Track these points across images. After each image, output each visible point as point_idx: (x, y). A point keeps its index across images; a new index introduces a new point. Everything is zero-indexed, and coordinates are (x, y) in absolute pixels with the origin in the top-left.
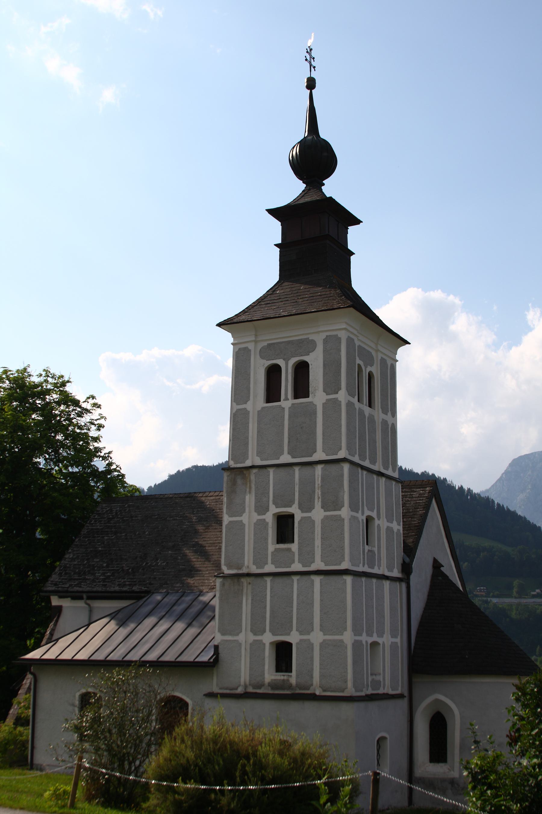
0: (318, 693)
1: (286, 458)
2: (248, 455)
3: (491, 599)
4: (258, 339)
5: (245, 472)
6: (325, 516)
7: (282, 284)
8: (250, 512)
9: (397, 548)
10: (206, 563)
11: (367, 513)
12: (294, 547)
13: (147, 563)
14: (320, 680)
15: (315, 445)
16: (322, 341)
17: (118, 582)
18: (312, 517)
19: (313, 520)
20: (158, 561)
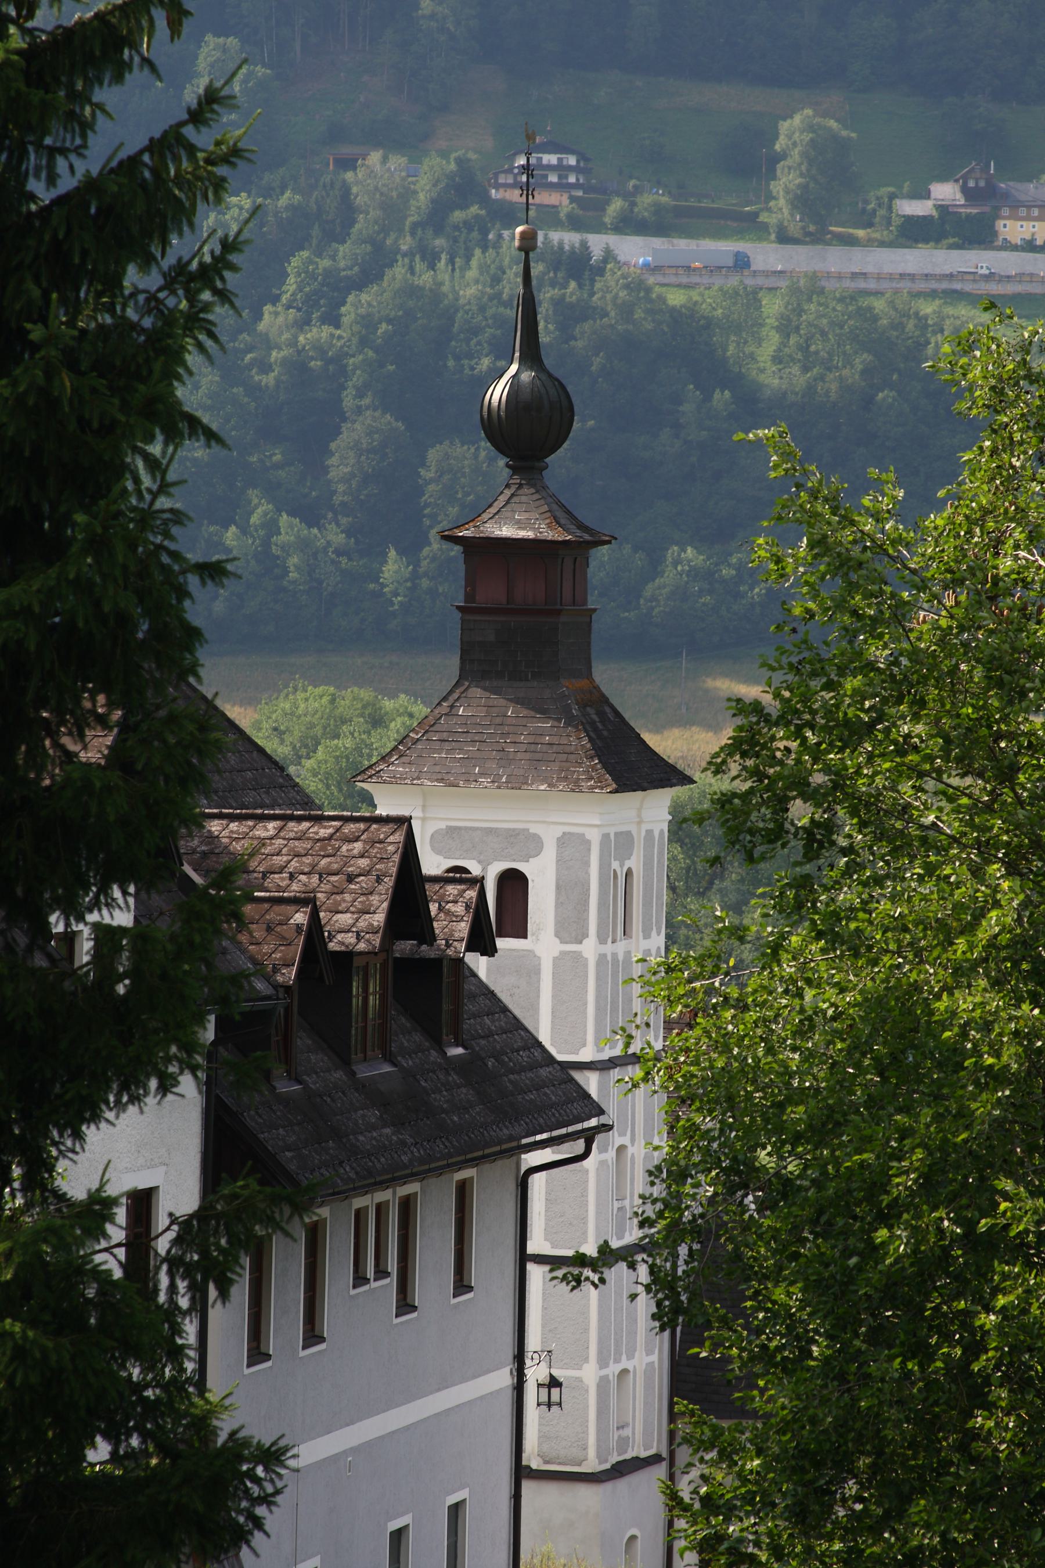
3: (612, 240)
14: (540, 1444)
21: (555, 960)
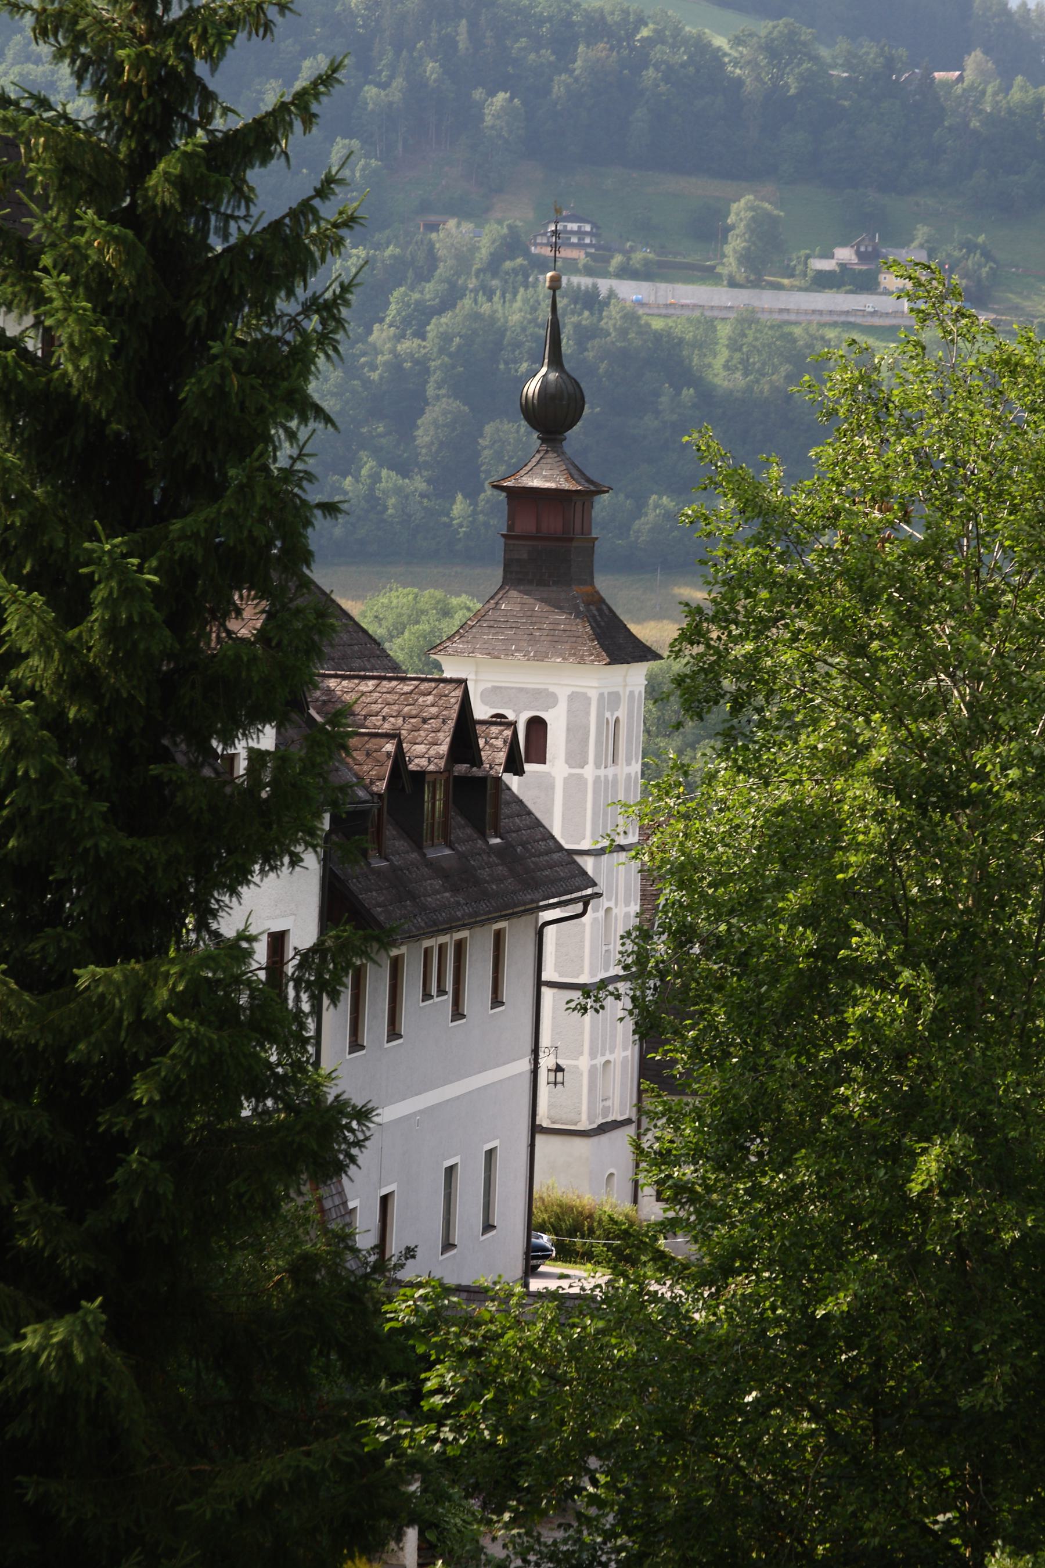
0: (545, 1125)
3: (614, 283)
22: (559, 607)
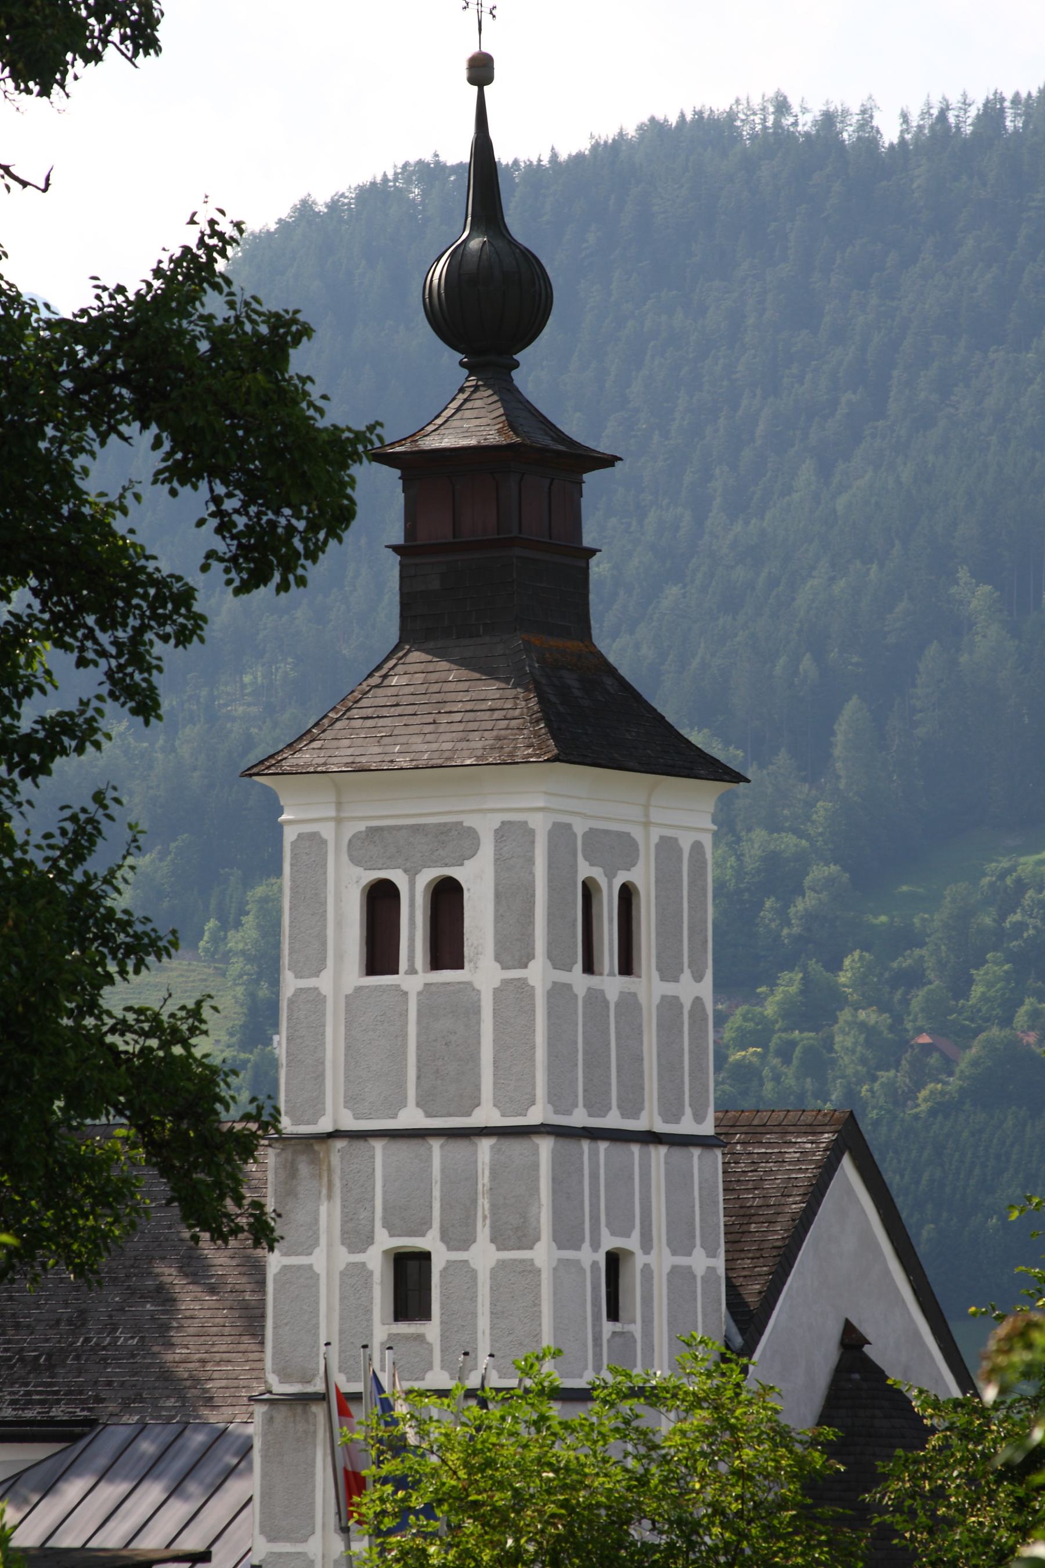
1: (411, 1117)
2: (324, 1103)
4: (344, 815)
5: (317, 1147)
6: (498, 1261)
7: (405, 655)
8: (330, 1245)
9: (704, 1315)
10: (246, 1339)
11: (610, 1242)
12: (431, 1330)
13: (87, 1340)
15: (478, 1088)
16: (492, 834)
17: (11, 1393)
18: (471, 1262)
19: (473, 1270)
20: (118, 1334)
21: (496, 991)
22: (491, 673)
